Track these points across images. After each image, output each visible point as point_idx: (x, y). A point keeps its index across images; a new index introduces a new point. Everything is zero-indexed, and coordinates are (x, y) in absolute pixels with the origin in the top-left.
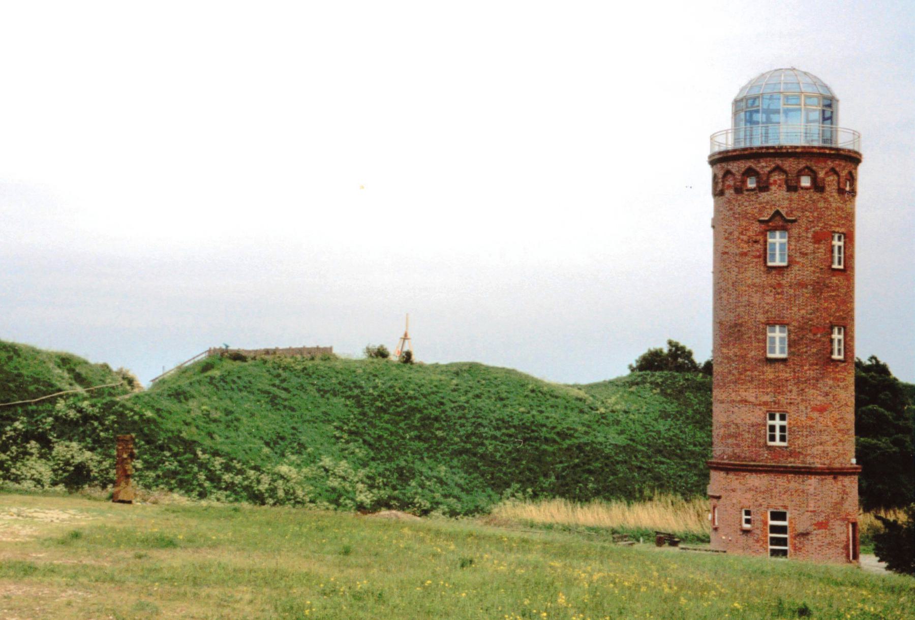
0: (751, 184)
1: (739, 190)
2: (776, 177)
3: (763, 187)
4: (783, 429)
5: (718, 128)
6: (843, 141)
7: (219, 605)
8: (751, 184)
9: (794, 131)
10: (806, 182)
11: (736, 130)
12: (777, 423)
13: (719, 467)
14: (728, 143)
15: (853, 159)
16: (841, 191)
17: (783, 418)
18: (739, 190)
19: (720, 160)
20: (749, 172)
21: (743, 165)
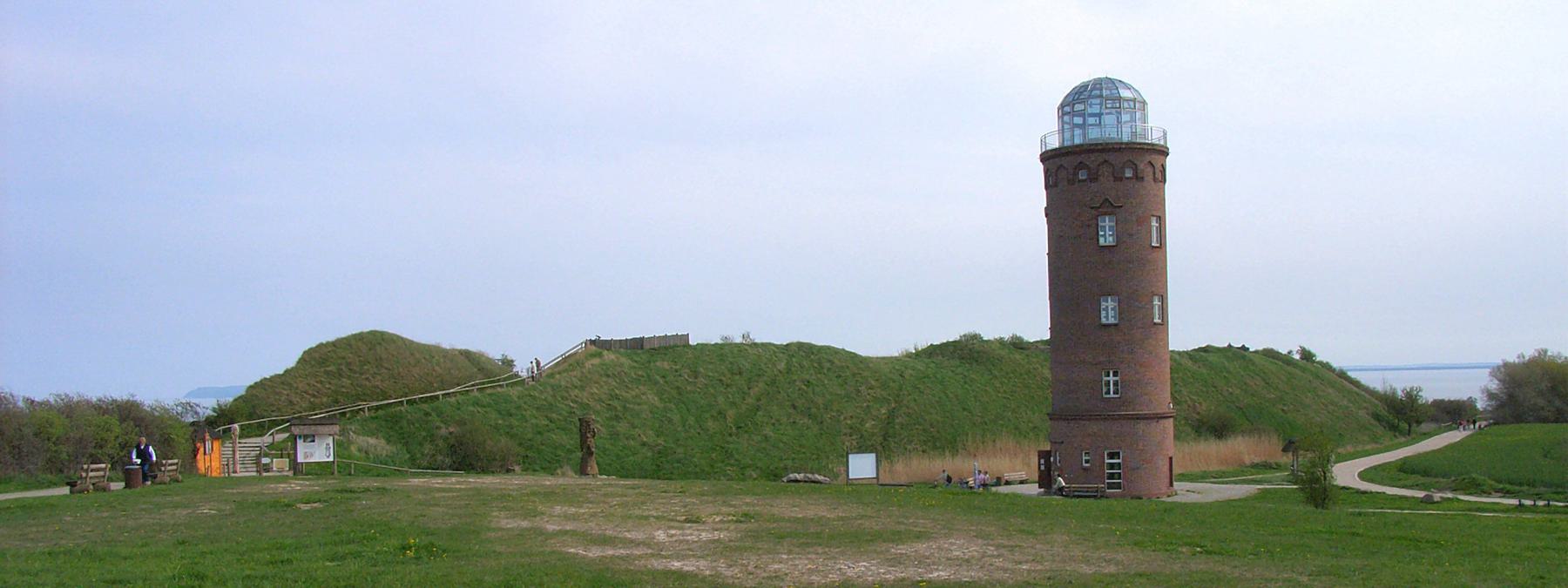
0: (1082, 175)
1: (1071, 182)
2: (1105, 170)
3: (1093, 178)
4: (1116, 384)
5: (1047, 130)
6: (1154, 138)
7: (773, 382)
8: (1082, 175)
9: (1109, 130)
10: (1129, 173)
11: (1062, 131)
12: (1112, 378)
13: (1184, 477)
14: (1054, 143)
15: (1164, 152)
16: (1155, 180)
17: (1115, 374)
18: (1071, 182)
19: (1046, 157)
20: (1081, 166)
21: (1076, 160)
